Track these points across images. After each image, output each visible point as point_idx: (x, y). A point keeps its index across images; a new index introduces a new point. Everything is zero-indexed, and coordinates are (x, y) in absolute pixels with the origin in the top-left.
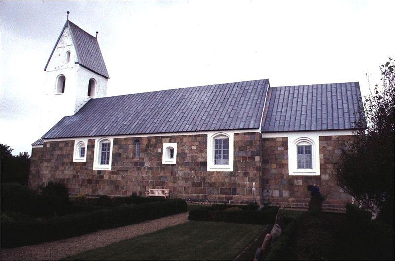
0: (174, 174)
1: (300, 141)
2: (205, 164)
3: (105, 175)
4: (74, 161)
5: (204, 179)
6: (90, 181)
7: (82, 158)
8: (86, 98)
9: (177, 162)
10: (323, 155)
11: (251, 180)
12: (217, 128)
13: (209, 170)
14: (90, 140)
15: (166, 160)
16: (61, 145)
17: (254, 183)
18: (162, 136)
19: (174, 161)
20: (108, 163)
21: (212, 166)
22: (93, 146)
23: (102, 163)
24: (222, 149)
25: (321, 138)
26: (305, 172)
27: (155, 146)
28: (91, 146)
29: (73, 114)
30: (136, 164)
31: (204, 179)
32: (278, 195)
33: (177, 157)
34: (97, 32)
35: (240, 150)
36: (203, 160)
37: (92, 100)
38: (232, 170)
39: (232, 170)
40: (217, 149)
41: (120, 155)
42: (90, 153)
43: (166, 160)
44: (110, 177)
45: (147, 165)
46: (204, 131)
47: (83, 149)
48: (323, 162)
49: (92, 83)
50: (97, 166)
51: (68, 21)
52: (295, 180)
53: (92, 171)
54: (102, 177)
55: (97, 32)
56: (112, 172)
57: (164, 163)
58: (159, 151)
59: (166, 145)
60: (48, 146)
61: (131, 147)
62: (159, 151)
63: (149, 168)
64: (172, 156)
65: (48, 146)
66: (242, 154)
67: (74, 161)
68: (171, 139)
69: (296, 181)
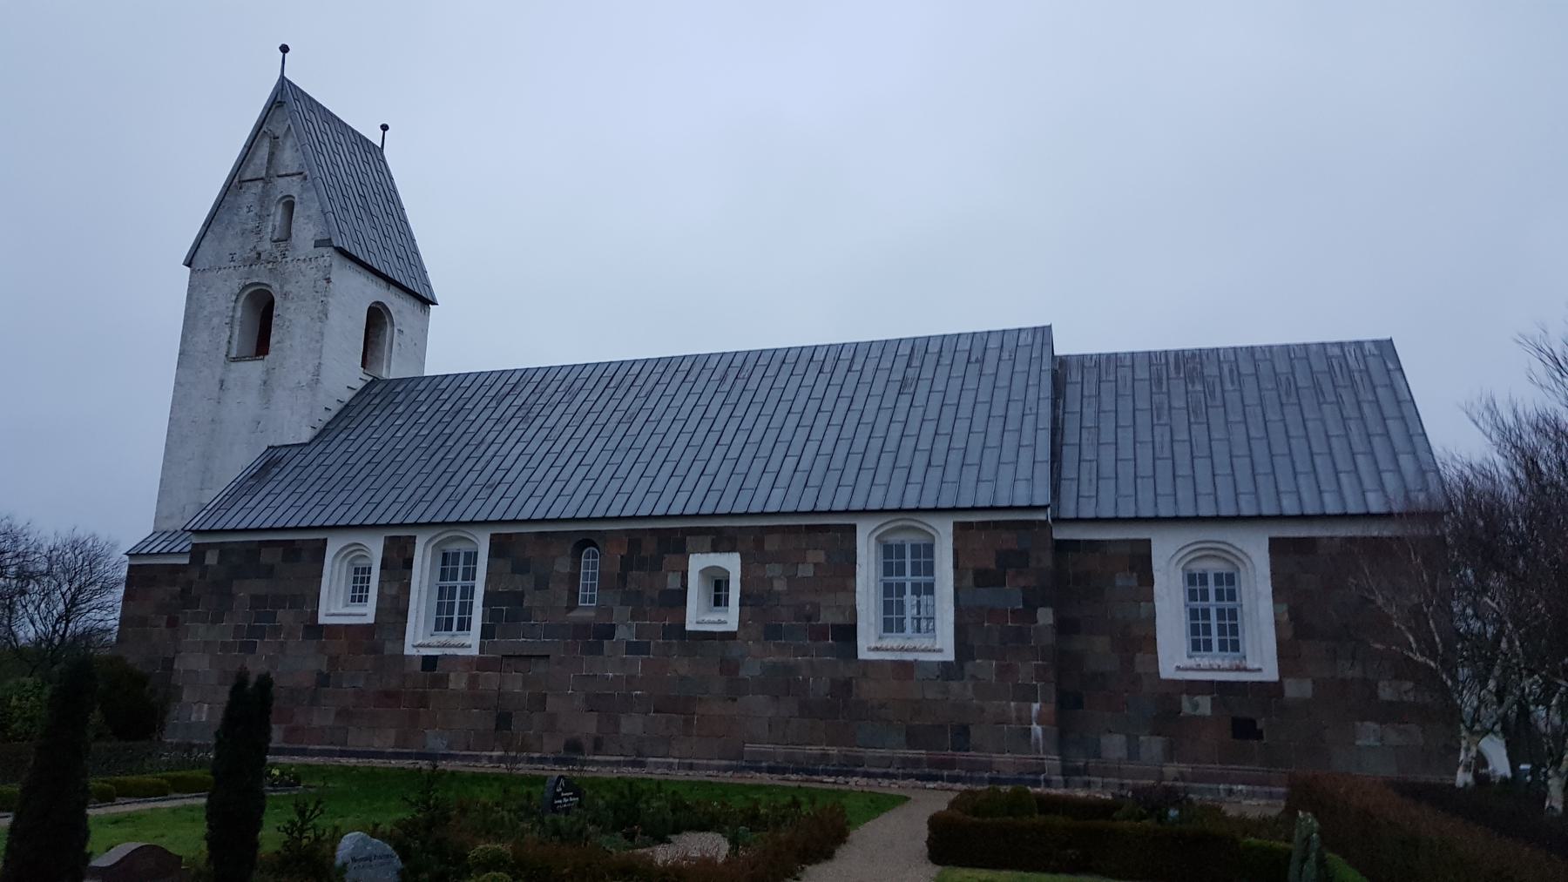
0: (729, 668)
1: (1198, 554)
2: (847, 633)
3: (452, 676)
4: (322, 620)
5: (847, 686)
6: (389, 697)
7: (357, 609)
8: (356, 377)
9: (742, 622)
10: (1285, 607)
11: (1028, 695)
12: (893, 504)
13: (863, 654)
14: (391, 543)
15: (698, 616)
16: (266, 557)
17: (1036, 707)
18: (682, 529)
19: (730, 619)
20: (464, 625)
21: (870, 643)
22: (408, 564)
23: (444, 625)
24: (908, 578)
25: (1276, 546)
26: (1214, 667)
27: (656, 565)
28: (398, 561)
29: (306, 435)
30: (581, 630)
31: (847, 686)
32: (1122, 753)
33: (741, 605)
34: (385, 128)
35: (977, 584)
36: (840, 620)
37: (375, 381)
38: (949, 656)
39: (949, 656)
40: (928, 579)
41: (518, 597)
42: (392, 590)
43: (698, 616)
44: (473, 681)
45: (624, 633)
46: (1137, 520)
47: (360, 577)
48: (1288, 634)
49: (377, 318)
50: (419, 637)
51: (282, 77)
52: (1184, 697)
53: (402, 658)
54: (442, 681)
55: (385, 128)
56: (480, 664)
57: (690, 626)
58: (673, 582)
59: (698, 563)
60: (211, 559)
61: (563, 566)
62: (673, 582)
63: (633, 648)
64: (720, 600)
65: (211, 559)
66: (987, 597)
67: (322, 620)
68: (721, 540)
69: (1186, 707)
